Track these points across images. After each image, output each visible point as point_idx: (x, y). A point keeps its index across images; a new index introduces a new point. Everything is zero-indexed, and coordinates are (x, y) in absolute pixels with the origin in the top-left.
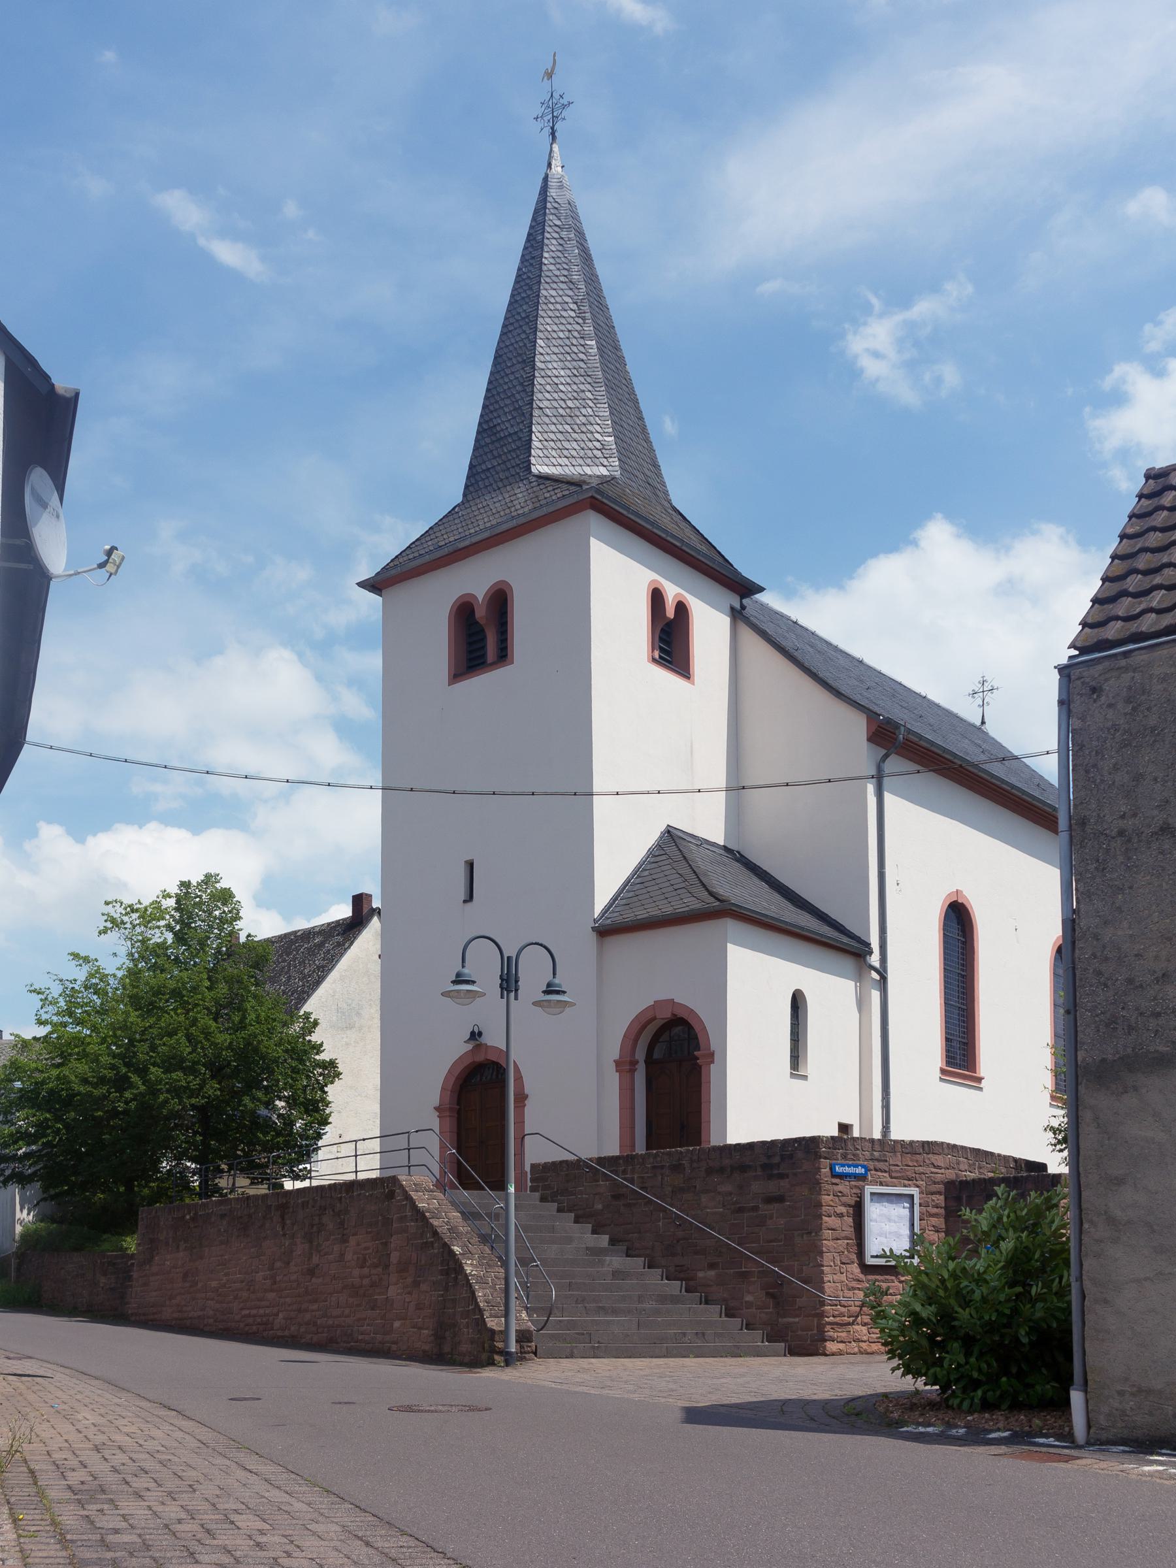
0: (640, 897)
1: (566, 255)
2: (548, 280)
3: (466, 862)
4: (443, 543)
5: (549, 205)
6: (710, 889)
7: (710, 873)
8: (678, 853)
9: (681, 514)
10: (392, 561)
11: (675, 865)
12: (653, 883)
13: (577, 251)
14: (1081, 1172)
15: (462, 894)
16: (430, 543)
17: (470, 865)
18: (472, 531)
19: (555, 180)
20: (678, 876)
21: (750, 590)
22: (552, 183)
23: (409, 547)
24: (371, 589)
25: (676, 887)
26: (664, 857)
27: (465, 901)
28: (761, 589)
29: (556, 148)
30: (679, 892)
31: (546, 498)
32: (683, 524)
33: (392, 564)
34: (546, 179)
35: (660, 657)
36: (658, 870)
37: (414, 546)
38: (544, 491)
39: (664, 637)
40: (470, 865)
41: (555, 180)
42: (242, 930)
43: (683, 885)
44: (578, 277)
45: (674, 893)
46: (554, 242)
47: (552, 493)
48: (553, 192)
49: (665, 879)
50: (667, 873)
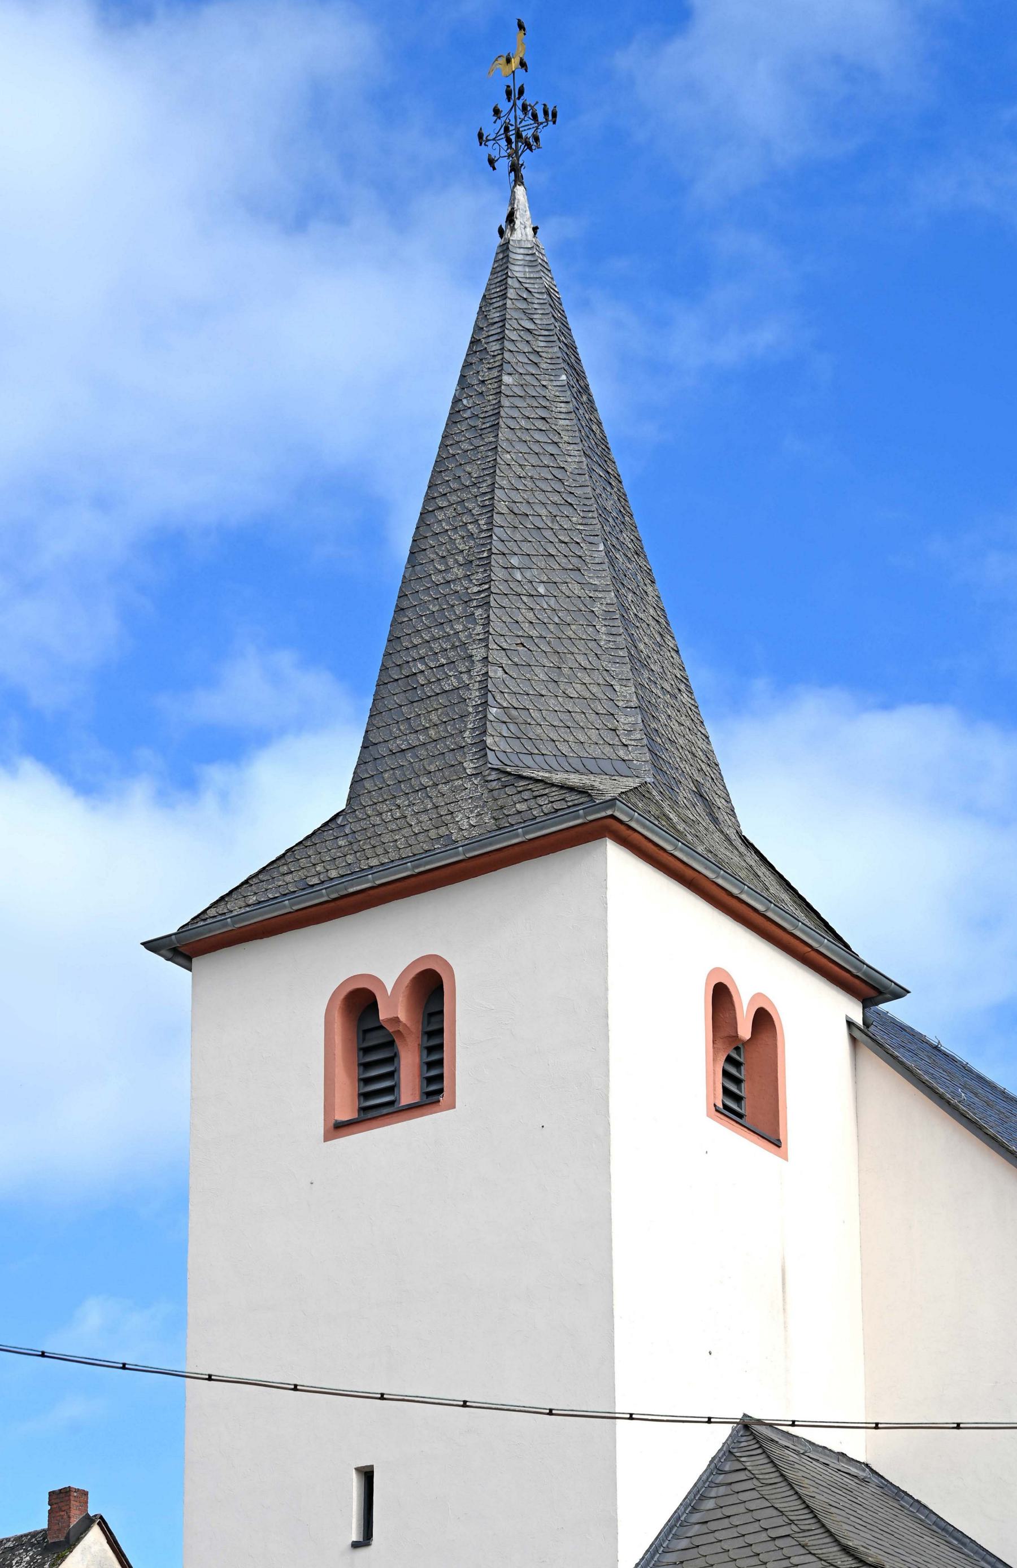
0: (703, 1550)
1: (544, 383)
2: (512, 424)
3: (358, 1470)
4: (315, 880)
5: (511, 293)
6: (842, 1541)
7: (833, 1510)
8: (769, 1468)
9: (757, 852)
10: (214, 905)
11: (766, 1491)
12: (725, 1523)
13: (564, 377)
14: (354, 881)
15: (355, 1534)
16: (288, 878)
17: (367, 1475)
18: (374, 862)
19: (522, 251)
20: (775, 1513)
21: (880, 993)
22: (517, 256)
23: (246, 882)
24: (170, 955)
25: (774, 1533)
26: (742, 1476)
27: (356, 1545)
28: (899, 993)
29: (520, 191)
30: (779, 1543)
31: (519, 812)
32: (762, 871)
33: (212, 912)
34: (505, 248)
35: (725, 1107)
36: (733, 1499)
37: (255, 880)
38: (515, 798)
39: (733, 1070)
40: (367, 1475)
41: (522, 251)
42: (526, 71)
43: (748, 1485)
44: (567, 422)
45: (771, 1546)
46: (522, 359)
47: (532, 803)
48: (518, 270)
49: (748, 1518)
50: (752, 1506)
